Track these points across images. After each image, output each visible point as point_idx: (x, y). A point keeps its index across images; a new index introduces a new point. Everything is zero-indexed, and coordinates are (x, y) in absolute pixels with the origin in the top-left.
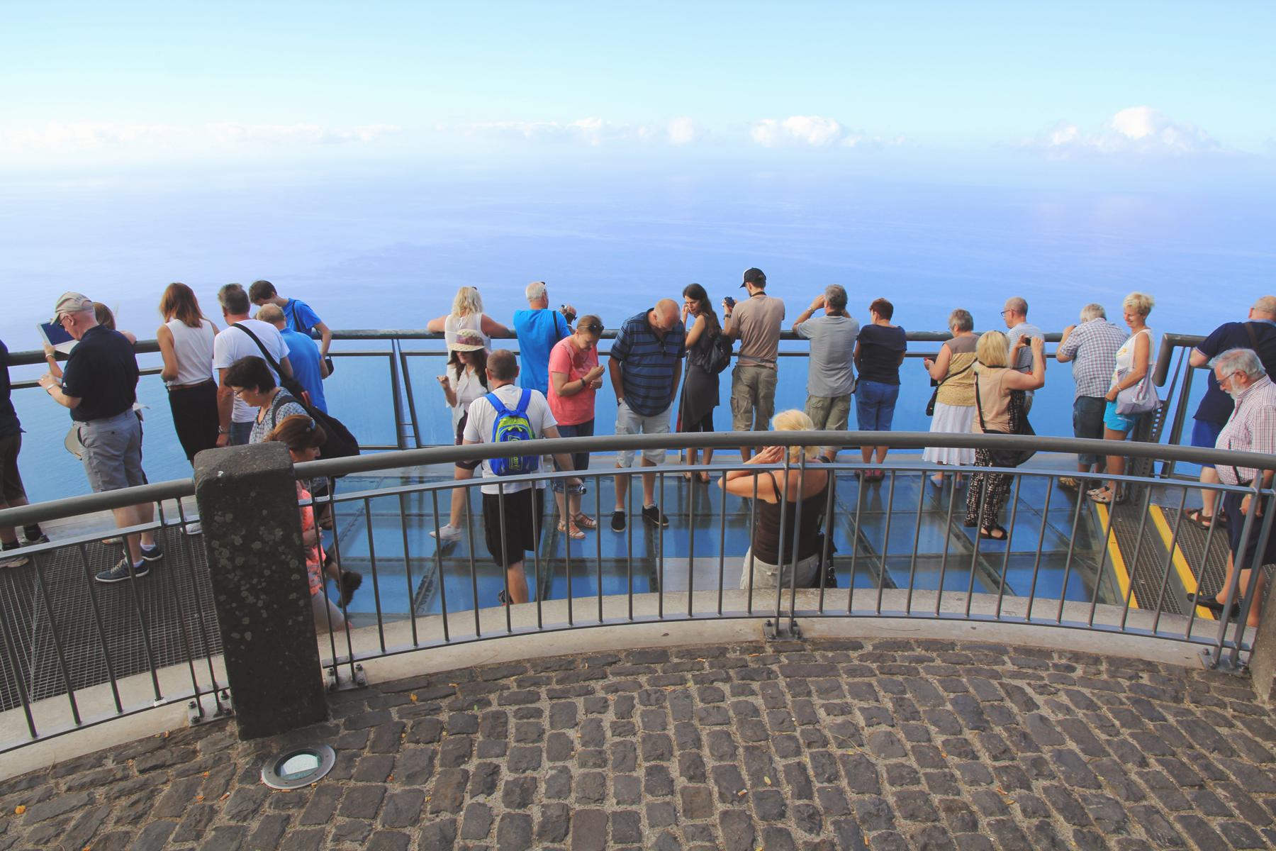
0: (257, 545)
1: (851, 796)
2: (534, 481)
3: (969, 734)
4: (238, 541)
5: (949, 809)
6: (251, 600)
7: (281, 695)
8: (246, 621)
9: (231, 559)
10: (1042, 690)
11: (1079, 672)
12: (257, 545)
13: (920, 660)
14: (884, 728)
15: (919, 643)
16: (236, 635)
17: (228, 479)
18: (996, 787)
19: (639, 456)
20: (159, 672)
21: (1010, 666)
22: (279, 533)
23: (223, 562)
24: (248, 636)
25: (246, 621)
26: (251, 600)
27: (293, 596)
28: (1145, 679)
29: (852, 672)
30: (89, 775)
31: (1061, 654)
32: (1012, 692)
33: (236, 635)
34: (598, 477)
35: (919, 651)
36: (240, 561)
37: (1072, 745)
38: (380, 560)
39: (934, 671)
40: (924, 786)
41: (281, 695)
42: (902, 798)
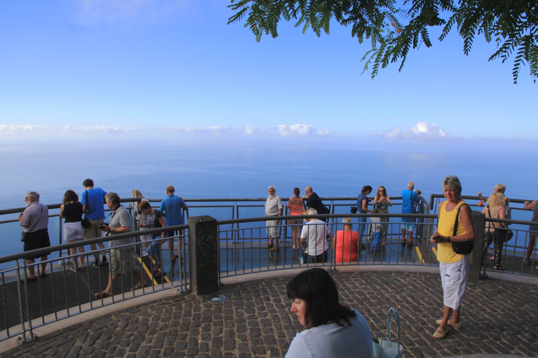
0: (207, 240)
1: (359, 297)
2: (131, 246)
3: (385, 286)
4: (203, 238)
5: (382, 298)
6: (204, 255)
7: (208, 281)
8: (202, 261)
9: (201, 243)
10: (402, 278)
11: (412, 275)
12: (207, 240)
13: (370, 275)
14: (364, 286)
15: (369, 272)
16: (200, 265)
17: (203, 222)
18: (393, 294)
19: (235, 225)
20: (70, 309)
21: (394, 275)
22: (212, 237)
23: (199, 244)
24: (202, 265)
25: (202, 261)
26: (204, 255)
27: (214, 254)
28: (428, 276)
29: (353, 277)
30: (161, 303)
31: (407, 272)
32: (395, 279)
33: (200, 265)
34: (51, 262)
35: (370, 273)
36: (203, 244)
37: (410, 287)
38: (222, 249)
39: (375, 276)
40: (376, 295)
41: (208, 281)
42: (371, 297)
